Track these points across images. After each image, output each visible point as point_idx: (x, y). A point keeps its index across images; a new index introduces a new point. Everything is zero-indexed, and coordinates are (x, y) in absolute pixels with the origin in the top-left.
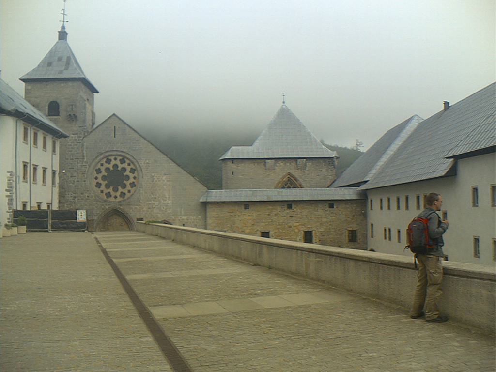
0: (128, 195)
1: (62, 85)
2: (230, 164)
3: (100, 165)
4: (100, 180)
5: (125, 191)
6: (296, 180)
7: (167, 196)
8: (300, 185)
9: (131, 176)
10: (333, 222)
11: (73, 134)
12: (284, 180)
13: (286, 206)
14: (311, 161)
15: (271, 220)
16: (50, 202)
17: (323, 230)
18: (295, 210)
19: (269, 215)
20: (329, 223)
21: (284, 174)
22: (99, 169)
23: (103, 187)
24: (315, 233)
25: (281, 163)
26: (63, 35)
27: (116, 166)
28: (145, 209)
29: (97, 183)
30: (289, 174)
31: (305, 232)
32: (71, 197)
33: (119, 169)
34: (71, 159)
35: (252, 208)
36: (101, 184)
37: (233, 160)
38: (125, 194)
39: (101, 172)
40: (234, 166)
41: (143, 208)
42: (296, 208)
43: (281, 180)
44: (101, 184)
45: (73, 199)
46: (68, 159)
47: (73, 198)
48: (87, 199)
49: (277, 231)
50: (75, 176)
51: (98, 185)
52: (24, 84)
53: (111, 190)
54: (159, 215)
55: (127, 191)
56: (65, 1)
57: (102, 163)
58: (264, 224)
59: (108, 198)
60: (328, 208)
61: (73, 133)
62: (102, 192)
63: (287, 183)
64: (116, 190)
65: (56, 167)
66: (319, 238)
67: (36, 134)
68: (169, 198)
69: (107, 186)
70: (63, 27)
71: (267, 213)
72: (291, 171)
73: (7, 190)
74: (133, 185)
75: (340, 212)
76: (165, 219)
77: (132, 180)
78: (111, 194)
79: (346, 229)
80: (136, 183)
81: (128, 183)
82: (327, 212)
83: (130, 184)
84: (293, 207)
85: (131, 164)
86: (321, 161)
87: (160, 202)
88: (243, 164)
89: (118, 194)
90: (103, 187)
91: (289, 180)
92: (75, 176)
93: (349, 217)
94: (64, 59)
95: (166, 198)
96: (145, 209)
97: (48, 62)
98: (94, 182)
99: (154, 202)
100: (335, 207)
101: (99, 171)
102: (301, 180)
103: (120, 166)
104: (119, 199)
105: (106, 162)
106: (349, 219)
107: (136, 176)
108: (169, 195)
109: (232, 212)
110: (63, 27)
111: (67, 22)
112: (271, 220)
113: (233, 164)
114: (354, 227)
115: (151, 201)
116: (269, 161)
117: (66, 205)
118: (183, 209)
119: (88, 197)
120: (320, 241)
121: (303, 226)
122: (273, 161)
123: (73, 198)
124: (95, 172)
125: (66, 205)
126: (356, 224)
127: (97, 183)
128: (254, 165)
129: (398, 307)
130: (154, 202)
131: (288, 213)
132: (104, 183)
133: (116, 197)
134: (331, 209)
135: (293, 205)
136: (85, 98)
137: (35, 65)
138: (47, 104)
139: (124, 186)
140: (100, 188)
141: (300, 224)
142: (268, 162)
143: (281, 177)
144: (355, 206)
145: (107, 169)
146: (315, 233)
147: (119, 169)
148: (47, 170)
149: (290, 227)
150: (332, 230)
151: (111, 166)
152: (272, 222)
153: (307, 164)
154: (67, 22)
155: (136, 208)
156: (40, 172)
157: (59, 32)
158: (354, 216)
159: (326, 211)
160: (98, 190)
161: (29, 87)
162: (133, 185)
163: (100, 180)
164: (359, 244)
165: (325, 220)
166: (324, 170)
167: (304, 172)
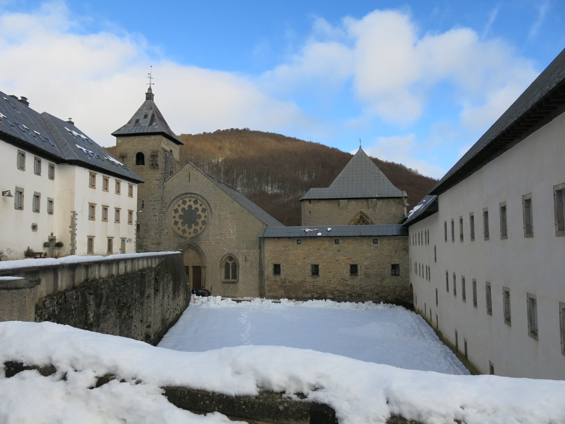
0: (199, 232)
1: (147, 139)
2: (307, 203)
3: (177, 205)
4: (177, 219)
5: (198, 228)
6: (367, 217)
7: (232, 232)
8: (372, 223)
9: (203, 215)
10: (377, 256)
11: (155, 180)
12: (357, 218)
13: (334, 242)
14: (382, 201)
15: (320, 255)
16: (298, 241)
17: (368, 264)
18: (342, 245)
19: (319, 249)
20: (374, 258)
21: (357, 212)
22: (177, 209)
23: (179, 225)
24: (361, 267)
25: (354, 203)
26: (150, 96)
27: (190, 206)
28: (213, 243)
29: (175, 221)
30: (361, 212)
31: (351, 265)
32: (154, 233)
33: (193, 209)
34: (154, 201)
35: (303, 242)
36: (178, 222)
37: (310, 200)
38: (197, 230)
39: (178, 212)
40: (311, 206)
41: (212, 243)
42: (342, 243)
43: (353, 218)
44: (178, 222)
45: (155, 235)
46: (151, 201)
47: (155, 234)
48: (167, 235)
49: (326, 264)
50: (157, 216)
51: (176, 223)
52: (115, 138)
53: (186, 227)
54: (225, 249)
55: (199, 228)
56: (151, 66)
57: (179, 204)
58: (314, 258)
59: (183, 233)
60: (372, 244)
61: (156, 179)
62: (179, 229)
63: (360, 221)
64: (190, 227)
65: (134, 208)
66: (363, 271)
67: (106, 180)
68: (233, 233)
69: (183, 224)
70: (150, 89)
71: (317, 248)
72: (363, 210)
73: (70, 227)
74: (204, 223)
75: (384, 247)
76: (229, 252)
77: (203, 219)
78: (186, 230)
79: (389, 263)
80: (206, 221)
81: (200, 221)
82: (372, 247)
83: (202, 222)
84: (340, 241)
85: (203, 205)
86: (392, 202)
87: (226, 236)
88: (319, 204)
89: (192, 230)
90: (179, 225)
91: (361, 218)
92: (157, 216)
93: (392, 252)
94: (149, 117)
95: (231, 234)
96: (213, 243)
97: (135, 121)
98: (173, 221)
99: (220, 238)
100: (379, 242)
101: (176, 211)
102: (372, 218)
103: (194, 207)
104: (193, 235)
105: (183, 203)
106: (392, 254)
107: (207, 215)
108: (233, 231)
109: (287, 247)
110: (150, 89)
111: (153, 84)
112: (320, 255)
113: (310, 204)
114: (396, 261)
115: (218, 236)
116: (342, 201)
117: (149, 240)
118: (245, 244)
119: (167, 233)
120: (365, 274)
121: (350, 260)
122: (346, 201)
123: (155, 234)
124: (174, 212)
125: (149, 240)
126: (399, 259)
127: (175, 221)
128: (330, 205)
129: (118, 327)
130: (220, 238)
131: (335, 247)
132: (180, 221)
133: (190, 233)
134: (376, 245)
135: (340, 240)
136: (168, 149)
137: (125, 122)
138: (135, 155)
139: (197, 224)
140: (177, 225)
141: (346, 258)
142: (342, 202)
143: (353, 215)
144: (397, 241)
145: (183, 209)
146: (361, 267)
147: (193, 209)
148: (121, 211)
149: (338, 261)
150: (376, 264)
151: (186, 207)
152: (321, 255)
153: (378, 203)
154: (153, 84)
155: (206, 243)
156: (111, 213)
157: (146, 94)
158: (396, 251)
159: (370, 246)
160: (176, 228)
161: (120, 141)
162: (204, 223)
163: (177, 219)
164: (402, 277)
165: (369, 255)
166: (394, 209)
167: (375, 210)
